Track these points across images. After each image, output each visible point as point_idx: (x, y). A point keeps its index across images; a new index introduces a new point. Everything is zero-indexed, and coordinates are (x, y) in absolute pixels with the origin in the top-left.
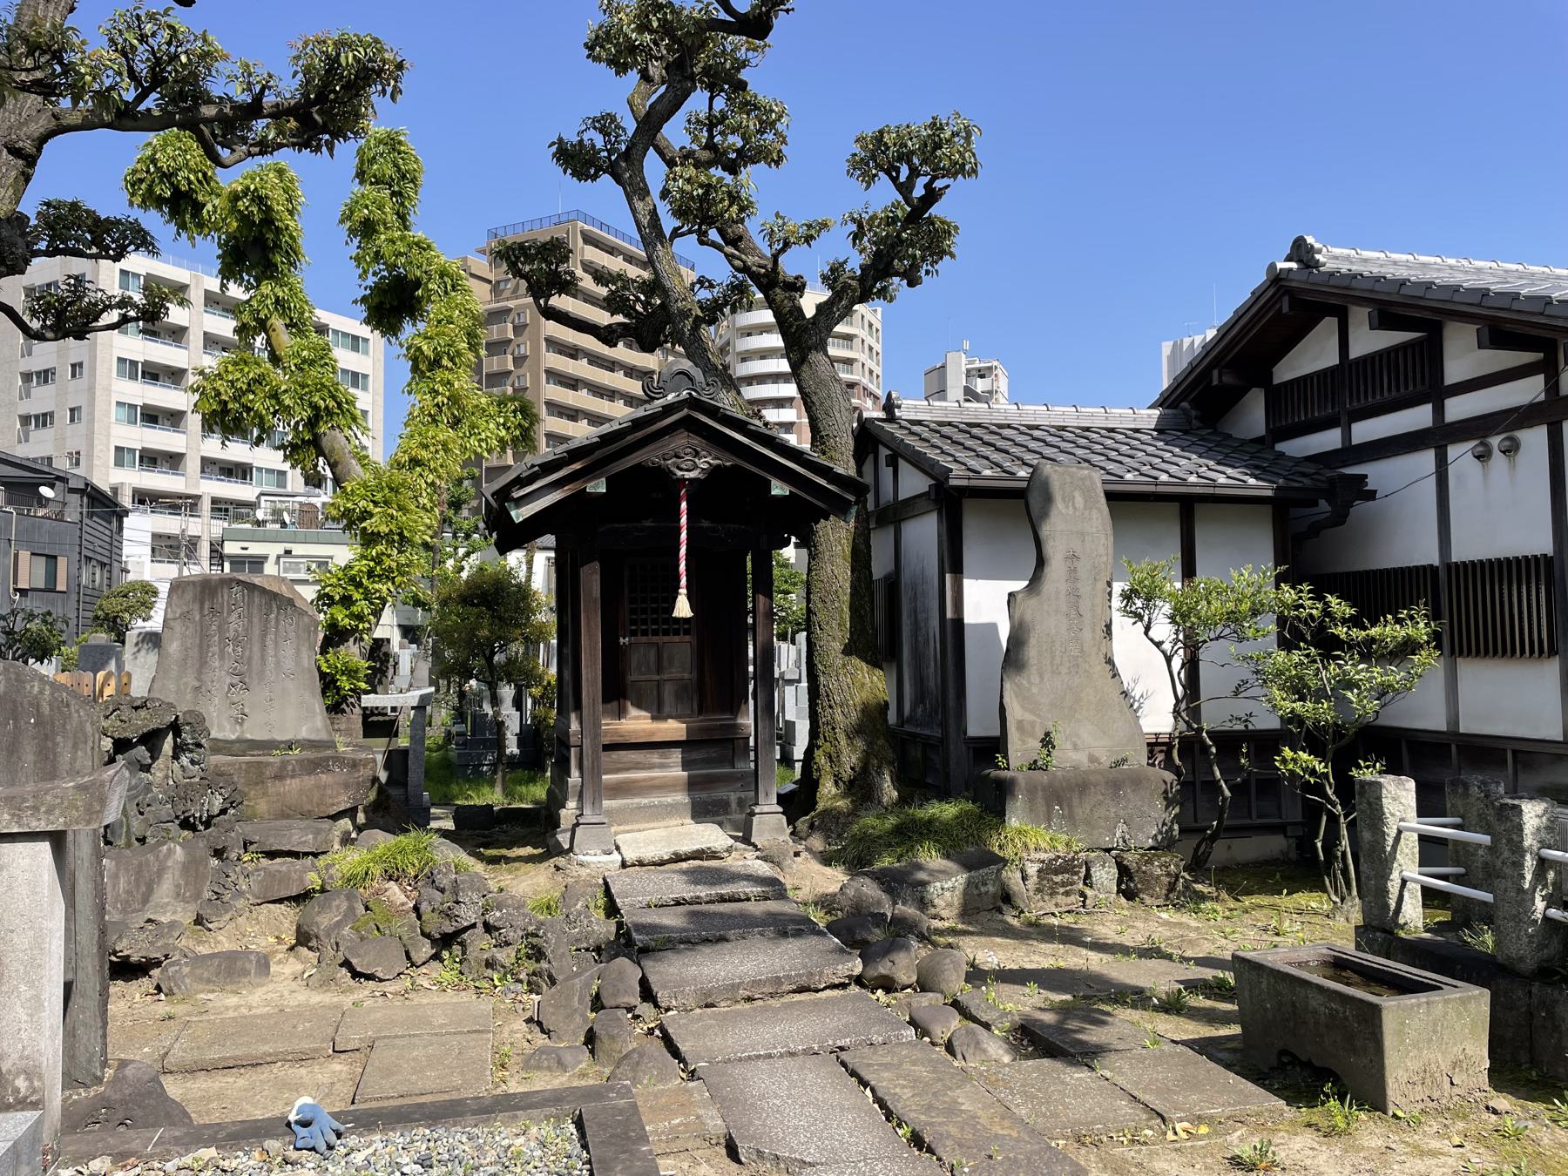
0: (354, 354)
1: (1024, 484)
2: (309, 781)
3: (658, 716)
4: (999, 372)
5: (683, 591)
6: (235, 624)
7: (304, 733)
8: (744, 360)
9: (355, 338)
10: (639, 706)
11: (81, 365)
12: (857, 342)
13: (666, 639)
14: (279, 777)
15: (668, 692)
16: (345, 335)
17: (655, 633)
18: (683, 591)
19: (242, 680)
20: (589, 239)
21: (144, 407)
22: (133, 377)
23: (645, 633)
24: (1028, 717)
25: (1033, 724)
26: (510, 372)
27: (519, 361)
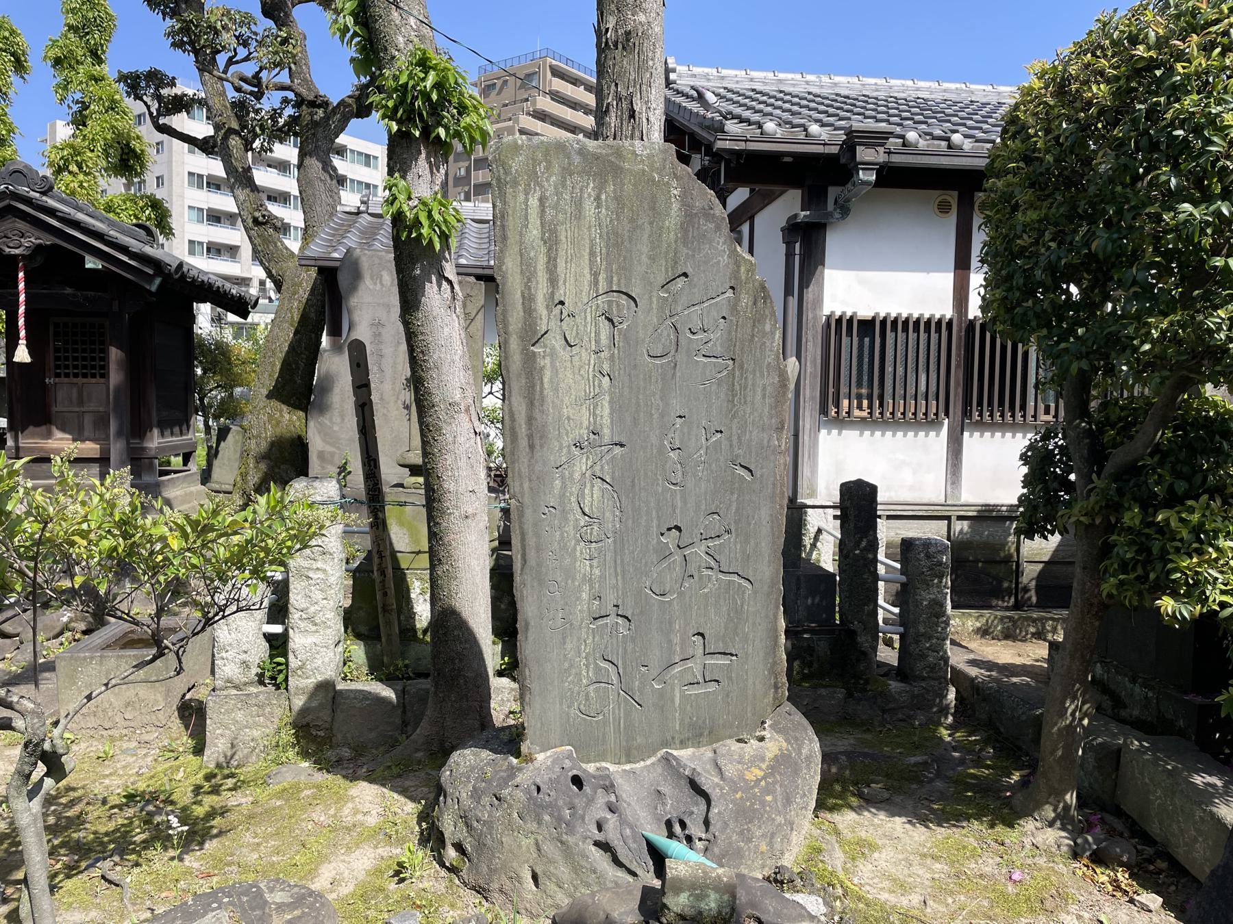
0: (366, 169)
1: (337, 264)
3: (79, 437)
5: (23, 342)
10: (63, 430)
11: (162, 177)
13: (85, 380)
15: (88, 421)
16: (360, 154)
17: (76, 376)
18: (23, 342)
20: (557, 73)
21: (209, 210)
22: (200, 187)
23: (67, 375)
24: (328, 448)
25: (332, 455)
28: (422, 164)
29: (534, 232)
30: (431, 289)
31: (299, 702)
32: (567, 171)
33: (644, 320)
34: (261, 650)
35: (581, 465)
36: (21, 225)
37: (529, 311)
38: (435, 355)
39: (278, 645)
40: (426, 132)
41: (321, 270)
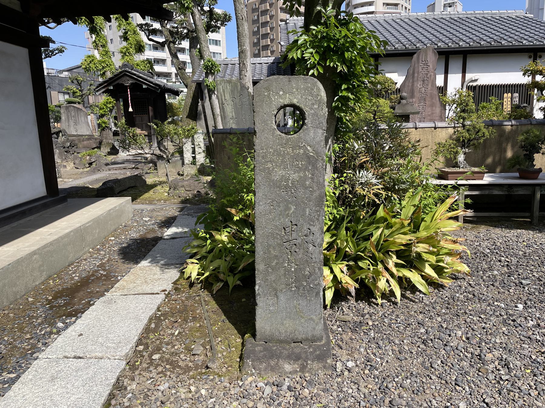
2: (88, 142)
4: (457, 4)
6: (73, 114)
7: (88, 133)
8: (355, 8)
9: (216, 41)
10: (139, 128)
12: (400, 6)
14: (83, 141)
19: (76, 123)
26: (269, 22)
27: (271, 17)
28: (210, 76)
29: (222, 90)
30: (213, 96)
31: (198, 167)
32: (225, 83)
33: (237, 101)
34: (191, 159)
35: (231, 121)
36: (128, 78)
37: (222, 101)
38: (215, 107)
39: (194, 158)
40: (210, 71)
41: (197, 83)
